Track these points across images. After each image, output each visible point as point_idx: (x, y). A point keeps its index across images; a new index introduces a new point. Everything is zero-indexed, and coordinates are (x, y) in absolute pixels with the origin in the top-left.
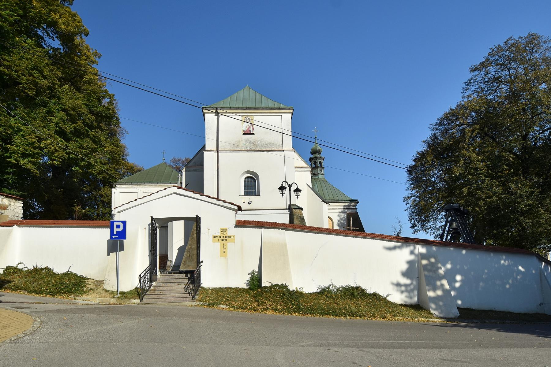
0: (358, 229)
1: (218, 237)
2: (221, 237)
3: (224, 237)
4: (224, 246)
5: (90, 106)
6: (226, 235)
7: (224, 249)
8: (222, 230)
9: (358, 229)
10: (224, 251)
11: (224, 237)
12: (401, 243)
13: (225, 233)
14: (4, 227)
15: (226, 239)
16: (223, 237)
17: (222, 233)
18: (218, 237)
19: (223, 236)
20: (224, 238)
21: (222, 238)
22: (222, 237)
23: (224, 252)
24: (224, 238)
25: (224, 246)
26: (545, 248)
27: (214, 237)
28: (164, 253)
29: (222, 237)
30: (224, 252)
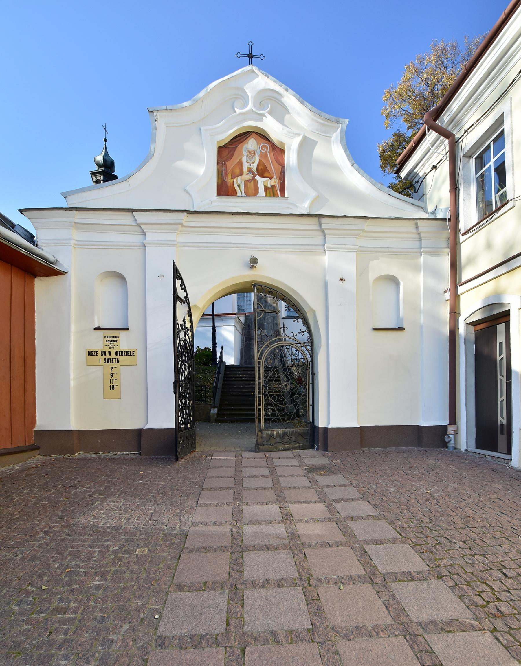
0: (181, 374)
1: (99, 354)
2: (105, 353)
3: (113, 354)
4: (112, 375)
5: (137, 659)
6: (117, 349)
7: (111, 381)
8: (107, 337)
9: (181, 374)
10: (112, 384)
11: (113, 354)
12: (201, 174)
13: (115, 344)
14: (209, 211)
15: (117, 357)
16: (110, 353)
17: (108, 343)
18: (99, 354)
19: (110, 350)
20: (113, 355)
21: (107, 356)
22: (107, 354)
23: (112, 388)
24: (113, 355)
25: (112, 375)
26: (173, 605)
27: (89, 354)
28: (16, 229)
29: (107, 354)
30: (112, 388)
